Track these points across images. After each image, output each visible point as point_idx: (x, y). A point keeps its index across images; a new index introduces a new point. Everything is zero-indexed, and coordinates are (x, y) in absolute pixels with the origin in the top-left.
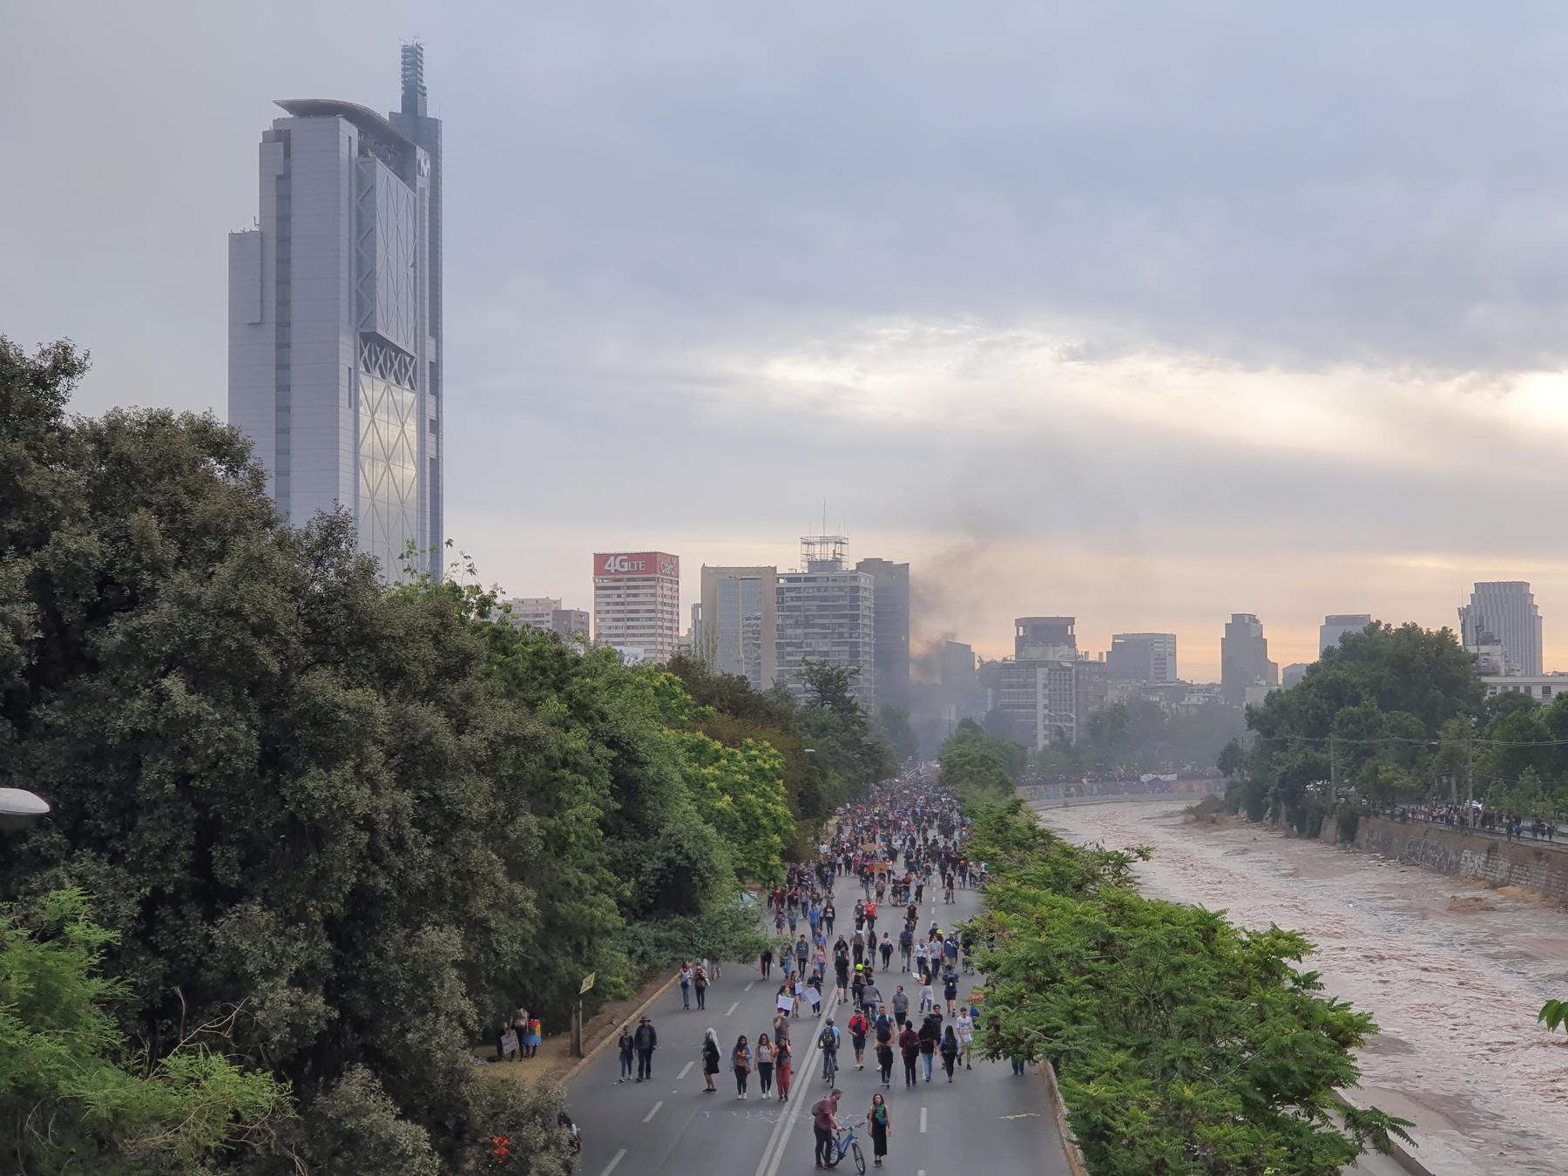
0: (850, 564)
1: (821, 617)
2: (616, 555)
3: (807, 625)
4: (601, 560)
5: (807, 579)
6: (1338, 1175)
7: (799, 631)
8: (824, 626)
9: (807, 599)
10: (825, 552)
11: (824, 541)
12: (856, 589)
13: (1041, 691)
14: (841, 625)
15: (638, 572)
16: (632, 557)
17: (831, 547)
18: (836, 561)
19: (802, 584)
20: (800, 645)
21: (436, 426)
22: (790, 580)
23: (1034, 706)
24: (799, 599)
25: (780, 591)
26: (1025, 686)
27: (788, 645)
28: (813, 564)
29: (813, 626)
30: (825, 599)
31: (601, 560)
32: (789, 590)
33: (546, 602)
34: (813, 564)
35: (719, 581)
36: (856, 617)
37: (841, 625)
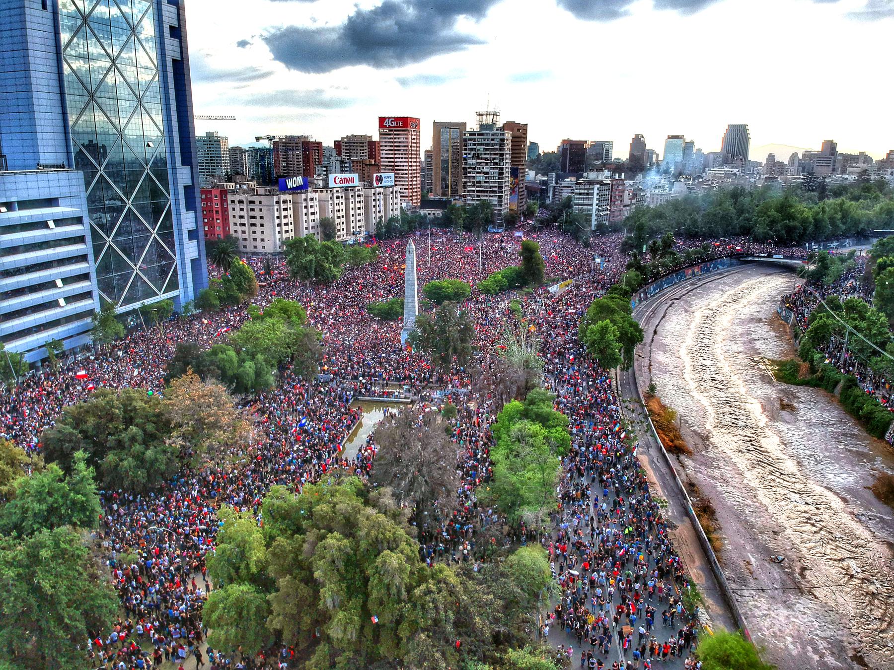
0: (500, 124)
1: (485, 154)
2: (389, 118)
3: (478, 158)
4: (382, 120)
5: (479, 135)
6: (420, 5)
7: (474, 161)
8: (486, 159)
9: (478, 144)
10: (488, 120)
11: (488, 114)
12: (503, 140)
13: (596, 197)
14: (494, 159)
15: (399, 127)
16: (397, 119)
17: (491, 117)
18: (494, 124)
19: (476, 137)
20: (474, 168)
21: (178, 32)
22: (470, 135)
23: (591, 205)
24: (474, 145)
25: (465, 140)
26: (588, 194)
27: (470, 168)
28: (482, 126)
29: (482, 159)
30: (487, 145)
31: (382, 120)
32: (470, 140)
33: (365, 137)
34: (482, 126)
35: (439, 128)
36: (502, 155)
37: (494, 159)
